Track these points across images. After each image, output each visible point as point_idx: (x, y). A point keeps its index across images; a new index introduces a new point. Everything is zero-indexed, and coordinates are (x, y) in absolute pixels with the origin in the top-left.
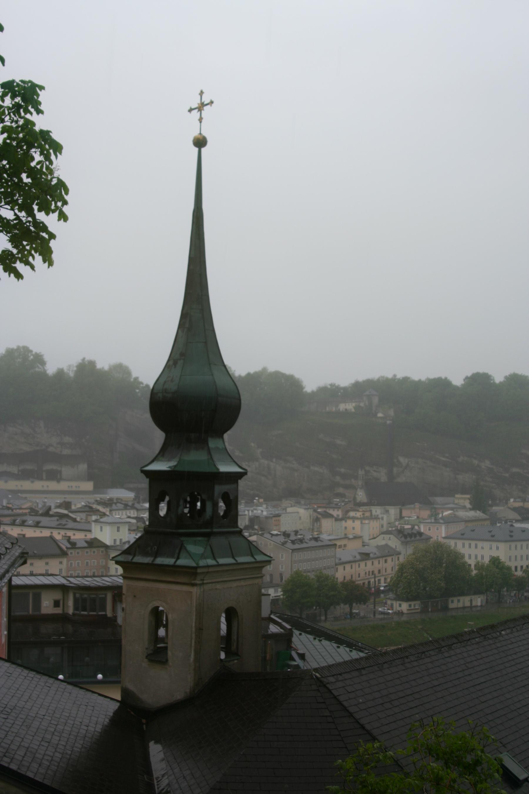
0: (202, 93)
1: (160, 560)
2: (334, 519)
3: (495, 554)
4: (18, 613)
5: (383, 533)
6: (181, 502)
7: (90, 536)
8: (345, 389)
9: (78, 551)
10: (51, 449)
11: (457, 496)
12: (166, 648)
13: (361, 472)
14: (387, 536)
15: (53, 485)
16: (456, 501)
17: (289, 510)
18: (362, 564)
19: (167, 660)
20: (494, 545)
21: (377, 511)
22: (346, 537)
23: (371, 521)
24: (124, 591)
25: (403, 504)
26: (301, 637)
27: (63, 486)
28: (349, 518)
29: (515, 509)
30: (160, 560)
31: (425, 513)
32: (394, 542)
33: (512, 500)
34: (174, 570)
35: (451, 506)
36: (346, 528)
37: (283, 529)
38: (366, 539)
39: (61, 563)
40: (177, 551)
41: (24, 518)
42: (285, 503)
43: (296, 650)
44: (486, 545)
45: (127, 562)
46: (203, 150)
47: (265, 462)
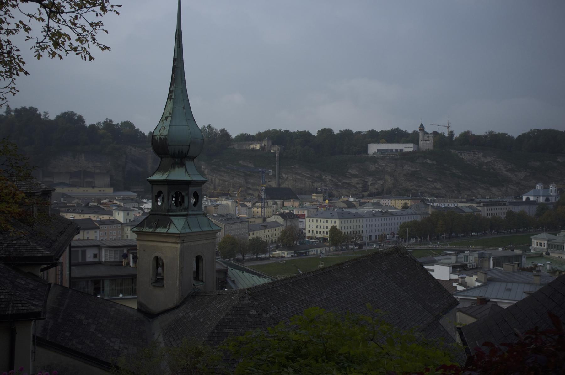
1: (158, 230)
3: (333, 224)
6: (171, 197)
7: (112, 218)
8: (253, 136)
12: (163, 279)
15: (90, 190)
18: (263, 231)
22: (254, 217)
24: (138, 248)
27: (96, 190)
28: (256, 207)
30: (158, 230)
31: (297, 204)
32: (280, 220)
33: (342, 197)
37: (220, 213)
39: (96, 232)
43: (230, 278)
44: (329, 220)
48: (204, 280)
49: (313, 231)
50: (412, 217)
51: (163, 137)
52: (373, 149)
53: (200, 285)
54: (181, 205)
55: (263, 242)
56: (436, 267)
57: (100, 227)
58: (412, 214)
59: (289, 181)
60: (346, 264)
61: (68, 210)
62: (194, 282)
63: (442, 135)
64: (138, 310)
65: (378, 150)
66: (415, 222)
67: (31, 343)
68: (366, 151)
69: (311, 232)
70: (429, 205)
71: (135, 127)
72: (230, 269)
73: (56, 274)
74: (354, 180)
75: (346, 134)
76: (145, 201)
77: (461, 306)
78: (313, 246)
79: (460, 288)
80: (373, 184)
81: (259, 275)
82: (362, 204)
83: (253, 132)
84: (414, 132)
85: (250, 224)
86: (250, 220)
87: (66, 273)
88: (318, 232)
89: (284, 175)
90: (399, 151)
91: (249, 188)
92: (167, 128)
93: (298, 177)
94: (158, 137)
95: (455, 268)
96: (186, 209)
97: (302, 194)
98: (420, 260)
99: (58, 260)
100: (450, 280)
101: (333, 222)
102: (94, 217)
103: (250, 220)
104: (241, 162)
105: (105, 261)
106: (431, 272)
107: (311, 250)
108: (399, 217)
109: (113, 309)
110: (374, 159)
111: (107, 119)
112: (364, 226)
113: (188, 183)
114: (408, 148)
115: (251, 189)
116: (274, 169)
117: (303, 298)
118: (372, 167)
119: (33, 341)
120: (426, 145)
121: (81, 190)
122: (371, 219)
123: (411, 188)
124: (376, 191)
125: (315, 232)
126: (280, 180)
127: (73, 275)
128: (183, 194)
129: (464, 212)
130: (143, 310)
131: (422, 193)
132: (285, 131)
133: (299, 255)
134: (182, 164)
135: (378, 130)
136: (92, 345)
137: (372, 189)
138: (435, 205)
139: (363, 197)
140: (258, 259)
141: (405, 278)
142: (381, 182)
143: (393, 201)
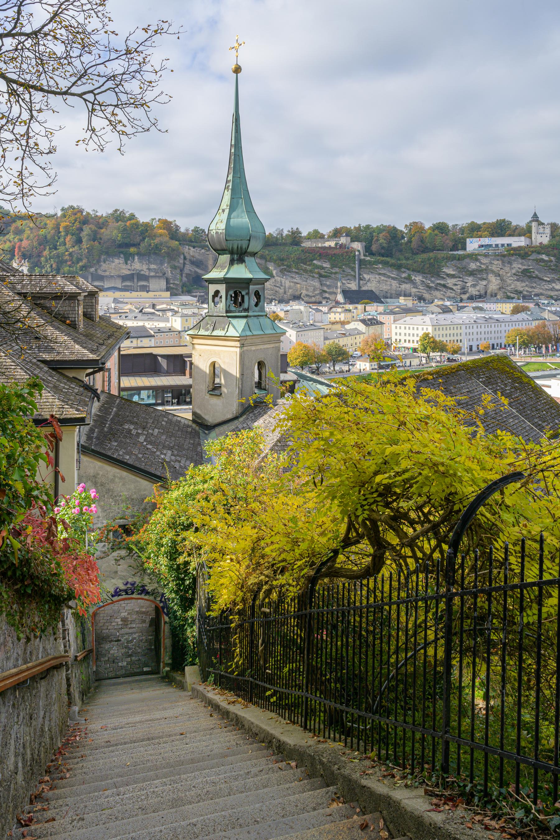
1: (215, 333)
4: (122, 385)
10: (142, 272)
14: (356, 323)
27: (151, 294)
29: (438, 306)
30: (215, 333)
32: (362, 327)
47: (278, 279)
51: (220, 231)
52: (472, 245)
54: (240, 305)
57: (156, 334)
59: (373, 282)
64: (194, 421)
67: (76, 451)
70: (545, 310)
73: (104, 381)
74: (450, 282)
80: (474, 286)
82: (460, 309)
90: (506, 245)
91: (325, 292)
93: (383, 278)
94: (214, 231)
96: (247, 310)
97: (387, 298)
98: (531, 374)
99: (103, 364)
101: (425, 329)
102: (148, 325)
106: (545, 389)
108: (507, 324)
110: (474, 257)
113: (248, 282)
114: (518, 242)
119: (78, 449)
120: (542, 238)
123: (522, 289)
124: (477, 293)
126: (361, 282)
127: (122, 385)
128: (244, 293)
130: (198, 420)
131: (536, 295)
134: (241, 260)
135: (479, 222)
137: (473, 291)
138: (553, 309)
139: (461, 300)
142: (484, 283)
143: (499, 305)
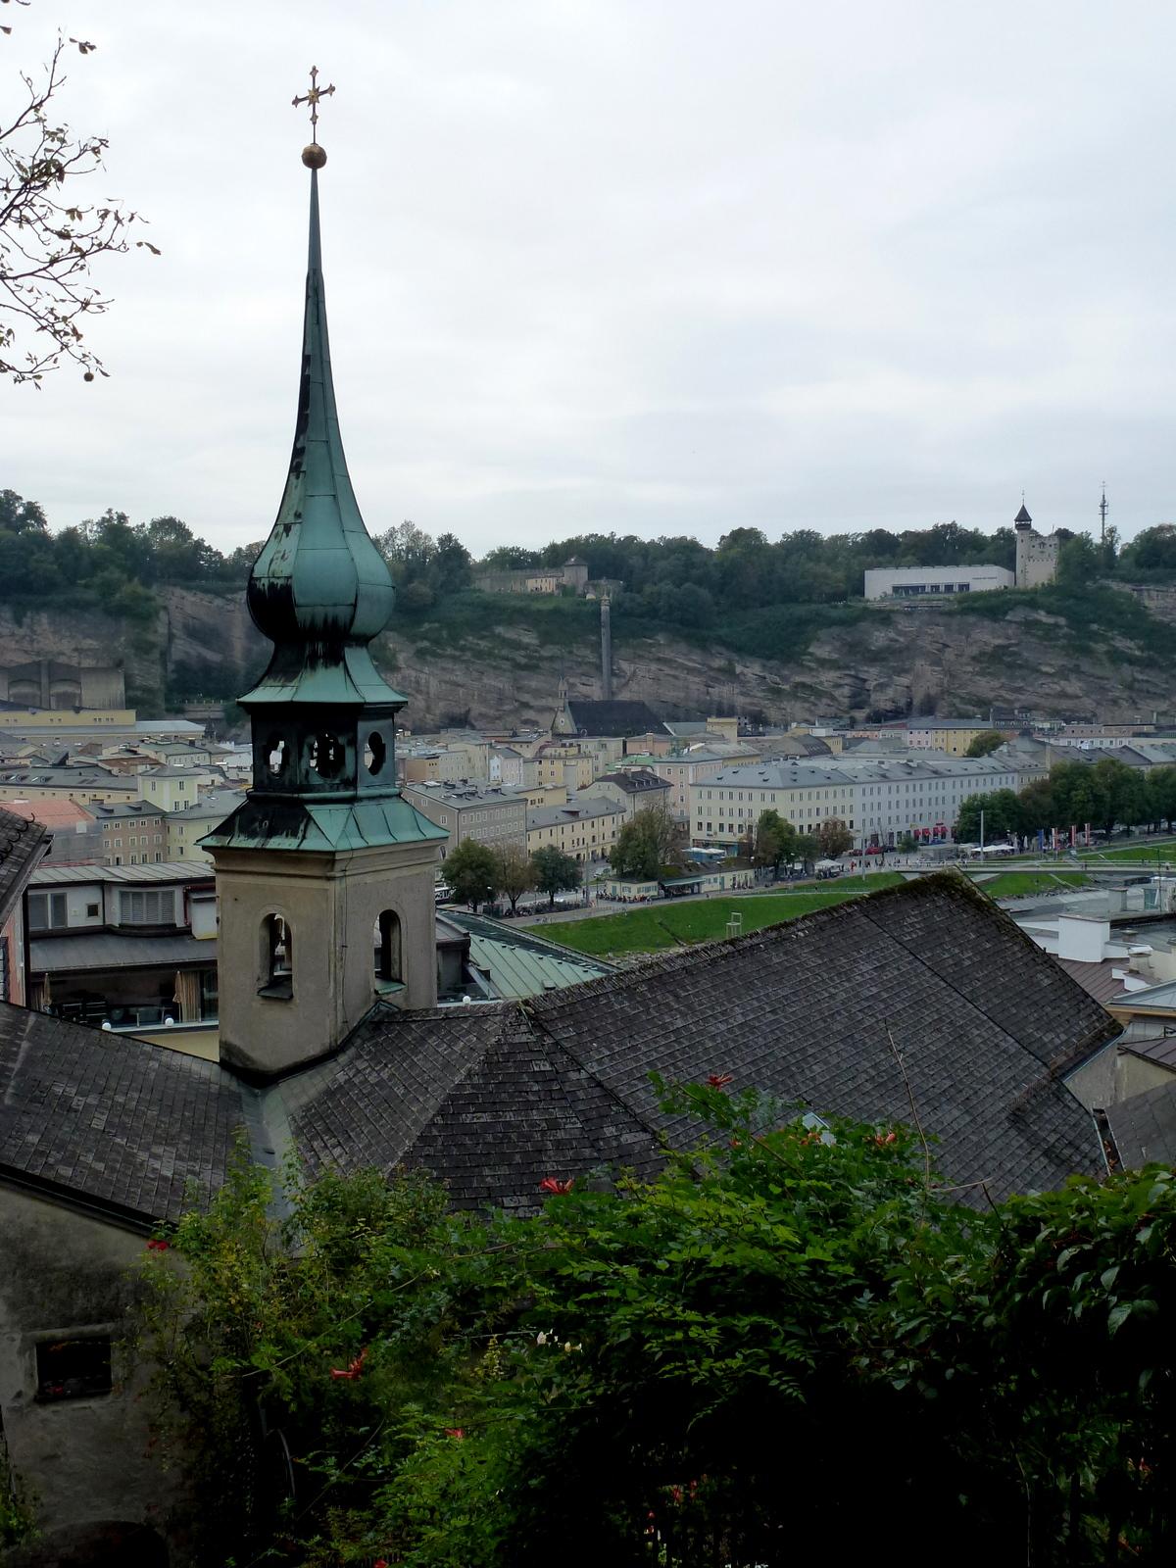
0: (314, 72)
1: (278, 843)
2: (522, 760)
5: (598, 780)
6: (306, 750)
8: (533, 555)
9: (116, 822)
10: (62, 660)
11: (709, 720)
12: (289, 978)
13: (562, 687)
15: (68, 717)
16: (709, 728)
17: (451, 747)
18: (568, 828)
19: (292, 996)
20: (768, 794)
21: (590, 744)
22: (541, 787)
23: (580, 761)
25: (629, 734)
26: (481, 945)
27: (86, 717)
28: (546, 758)
31: (663, 748)
32: (615, 792)
33: (794, 725)
34: (297, 857)
35: (701, 735)
36: (540, 773)
37: (443, 778)
38: (573, 789)
40: (302, 827)
41: (24, 773)
42: (446, 735)
45: (222, 848)
46: (319, 171)
48: (404, 979)
49: (709, 825)
50: (996, 778)
51: (280, 582)
52: (880, 583)
53: (394, 995)
55: (567, 860)
56: (1062, 925)
58: (995, 772)
60: (800, 926)
61: (8, 778)
62: (378, 985)
63: (1083, 542)
65: (896, 589)
66: (1006, 797)
68: (859, 589)
69: (705, 826)
71: (189, 535)
72: (475, 938)
74: (828, 677)
75: (804, 544)
76: (228, 746)
77: (1133, 1032)
78: (709, 865)
79: (1133, 985)
81: (558, 955)
83: (535, 541)
84: (1001, 531)
85: (530, 806)
86: (530, 797)
87: (18, 965)
88: (726, 827)
89: (624, 665)
90: (956, 589)
91: (526, 705)
92: (291, 557)
93: (667, 670)
94: (265, 582)
95: (1124, 926)
100: (1106, 961)
103: (530, 797)
104: (499, 630)
105: (121, 926)
107: (704, 878)
109: (154, 1064)
110: (883, 617)
111: (110, 511)
112: (858, 808)
114: (986, 579)
115: (531, 707)
116: (596, 647)
117: (680, 1023)
118: (879, 638)
120: (1038, 572)
121: (43, 718)
122: (875, 787)
124: (889, 706)
125: (715, 827)
126: (615, 681)
129: (1150, 763)
131: (1027, 709)
132: (627, 538)
133: (668, 894)
134: (335, 658)
136: (100, 1166)
137: (882, 701)
138: (1063, 742)
140: (552, 907)
141: (967, 963)
142: (905, 680)
